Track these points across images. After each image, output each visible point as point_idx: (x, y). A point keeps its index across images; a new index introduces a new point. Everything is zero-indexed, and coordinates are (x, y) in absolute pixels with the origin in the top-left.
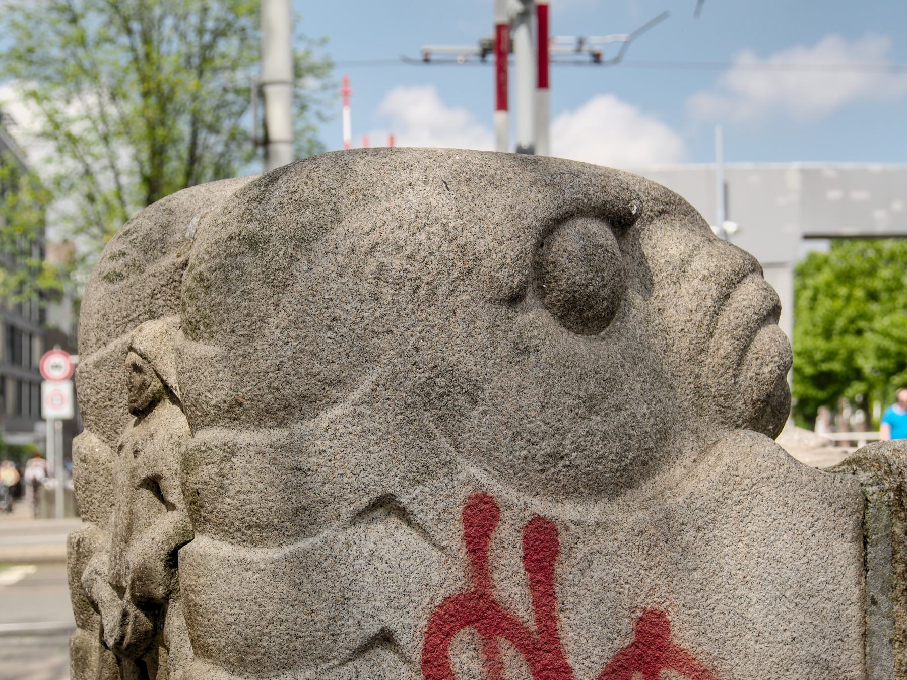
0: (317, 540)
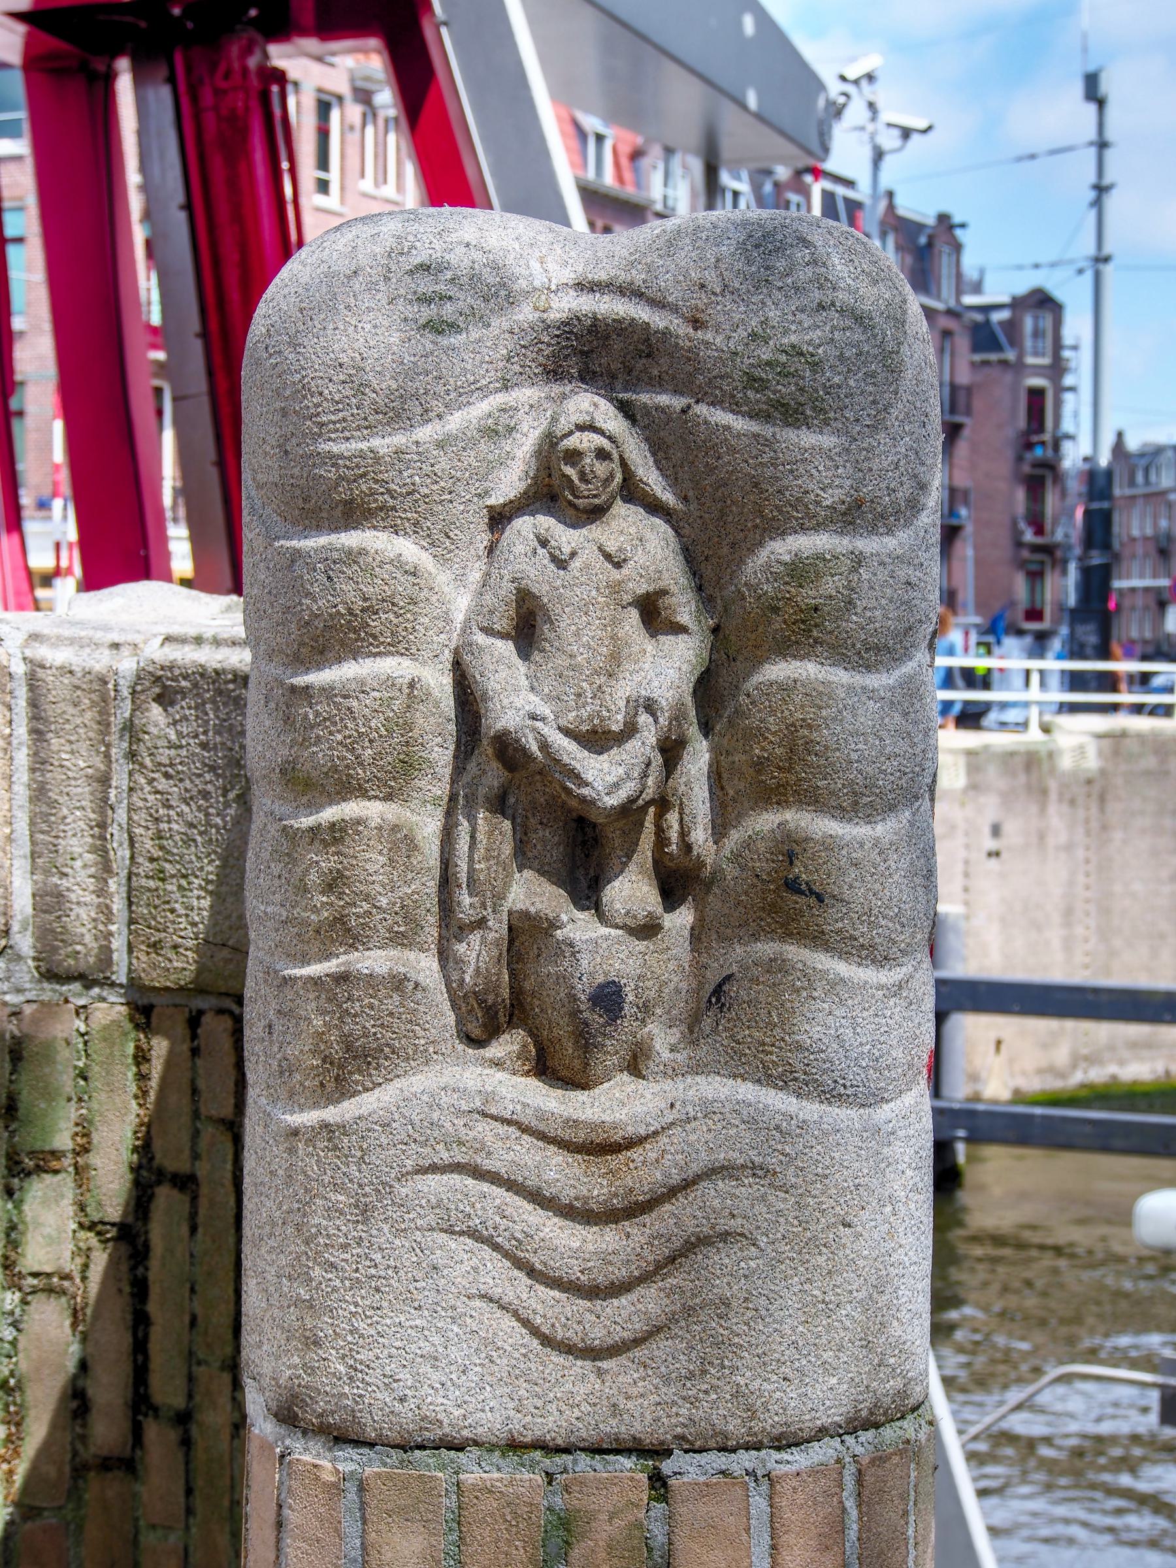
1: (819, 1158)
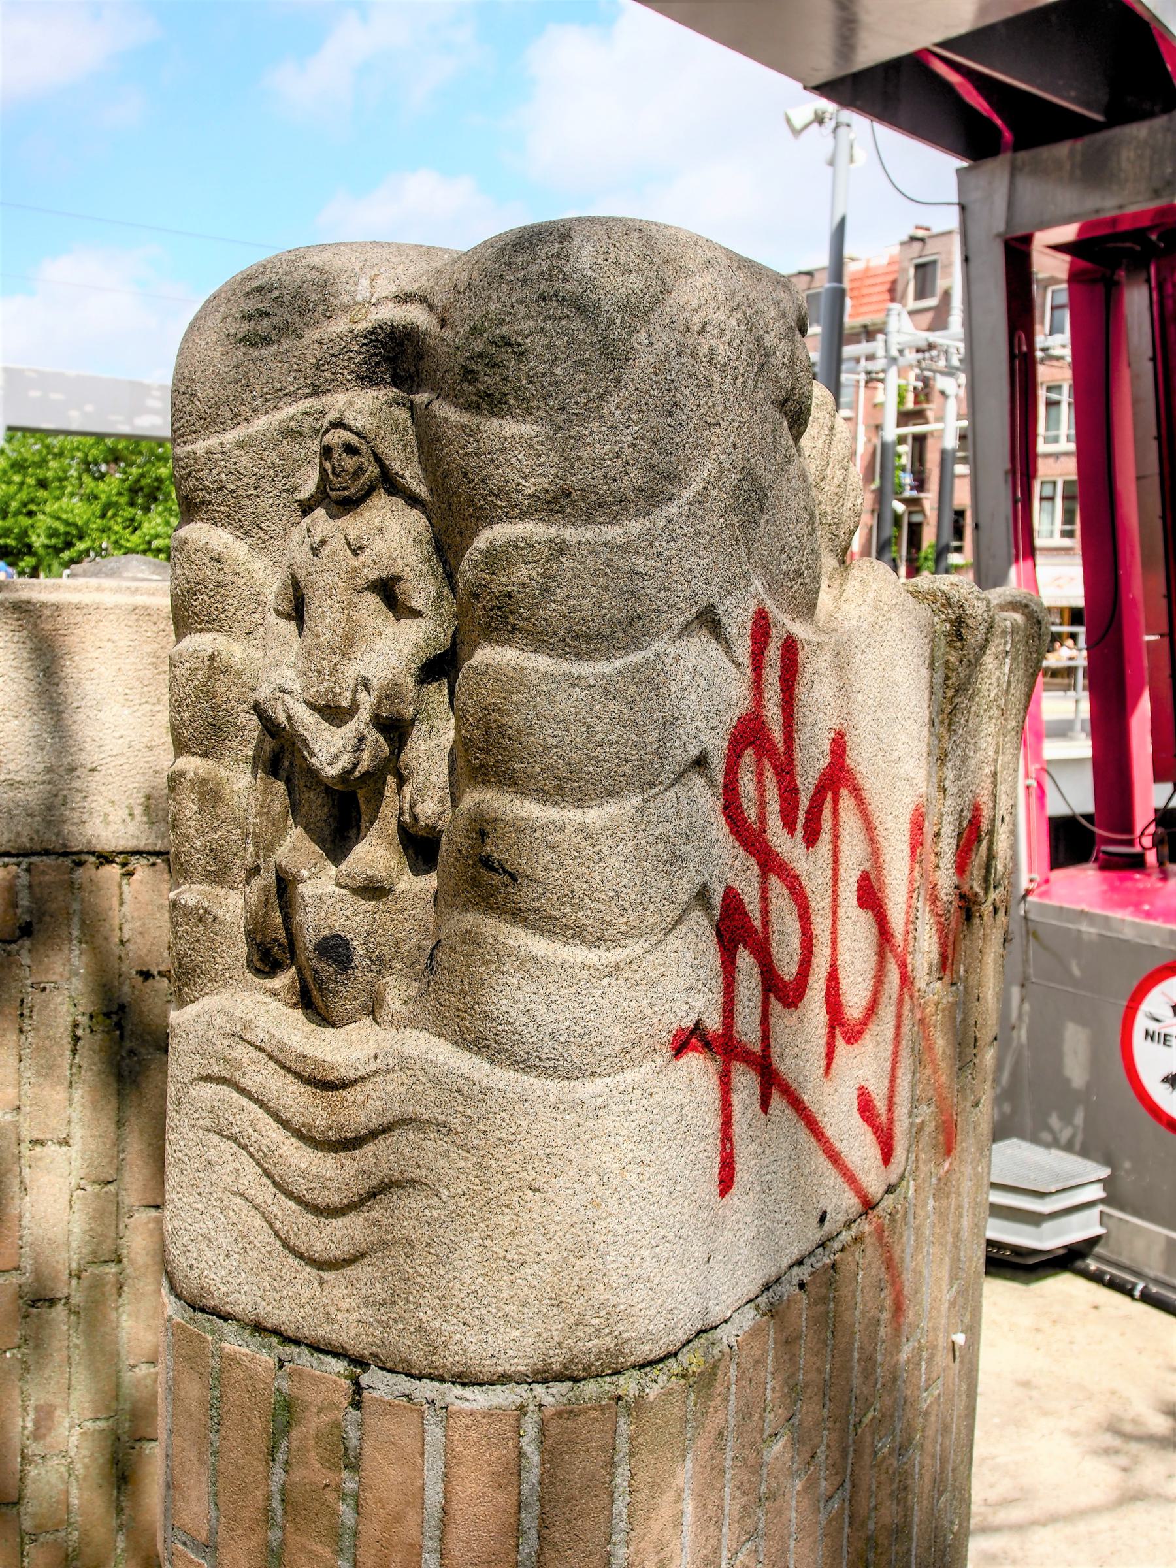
0: (649, 653)
1: (504, 1124)
